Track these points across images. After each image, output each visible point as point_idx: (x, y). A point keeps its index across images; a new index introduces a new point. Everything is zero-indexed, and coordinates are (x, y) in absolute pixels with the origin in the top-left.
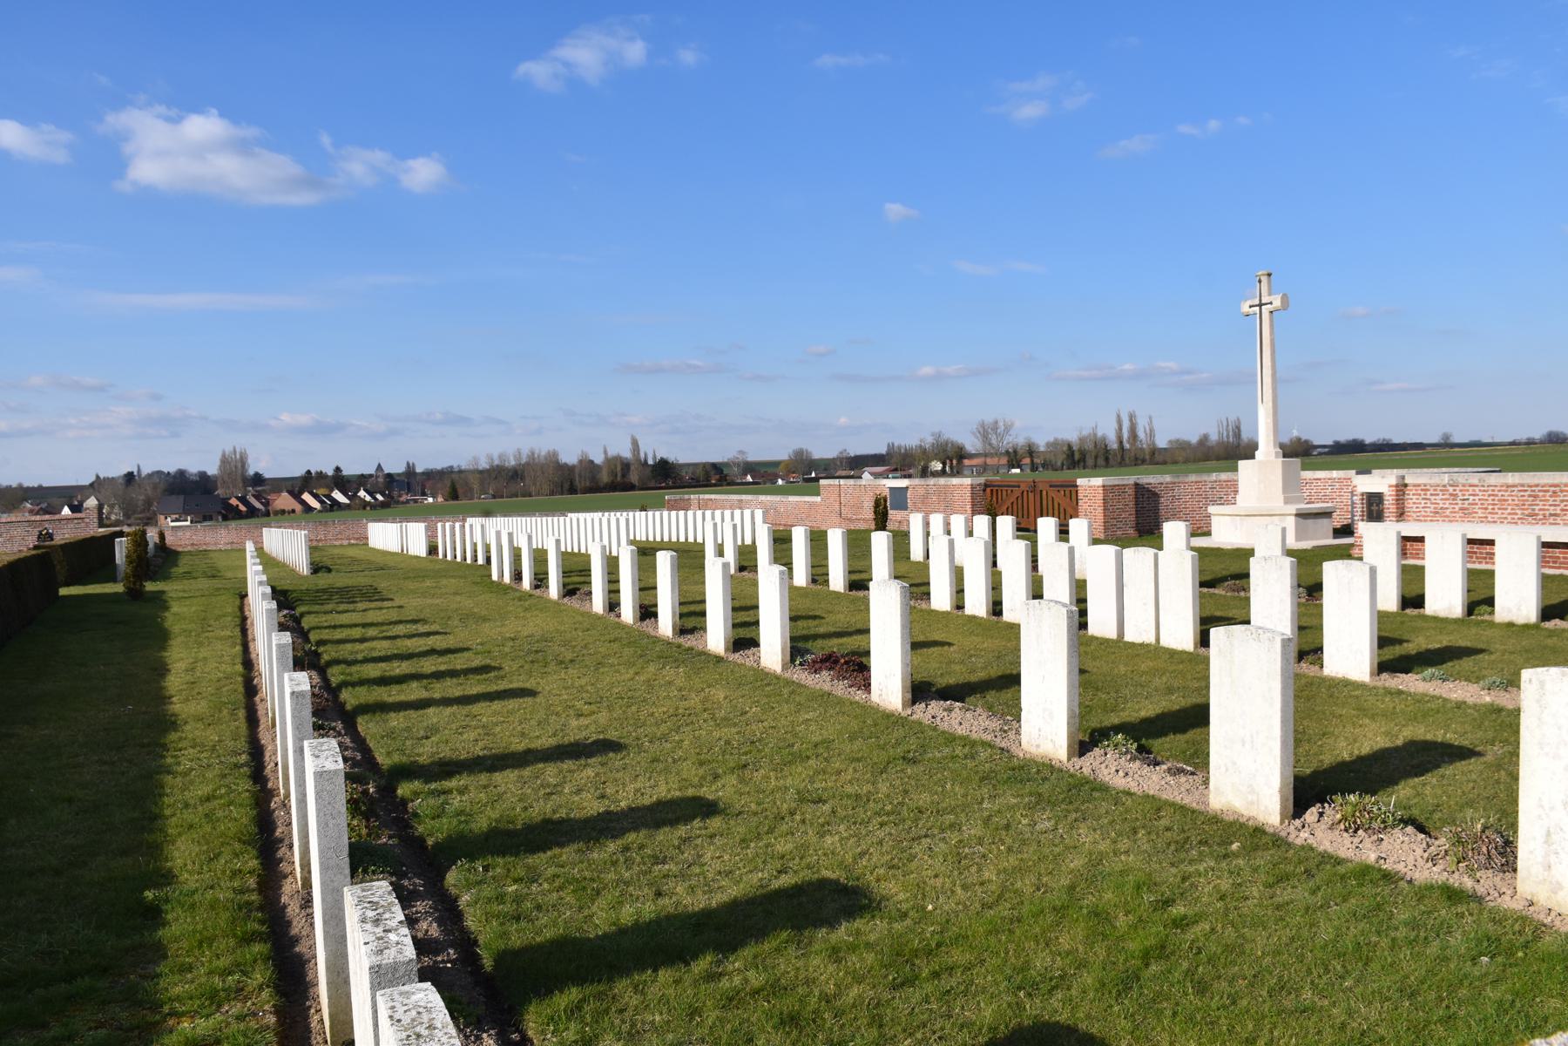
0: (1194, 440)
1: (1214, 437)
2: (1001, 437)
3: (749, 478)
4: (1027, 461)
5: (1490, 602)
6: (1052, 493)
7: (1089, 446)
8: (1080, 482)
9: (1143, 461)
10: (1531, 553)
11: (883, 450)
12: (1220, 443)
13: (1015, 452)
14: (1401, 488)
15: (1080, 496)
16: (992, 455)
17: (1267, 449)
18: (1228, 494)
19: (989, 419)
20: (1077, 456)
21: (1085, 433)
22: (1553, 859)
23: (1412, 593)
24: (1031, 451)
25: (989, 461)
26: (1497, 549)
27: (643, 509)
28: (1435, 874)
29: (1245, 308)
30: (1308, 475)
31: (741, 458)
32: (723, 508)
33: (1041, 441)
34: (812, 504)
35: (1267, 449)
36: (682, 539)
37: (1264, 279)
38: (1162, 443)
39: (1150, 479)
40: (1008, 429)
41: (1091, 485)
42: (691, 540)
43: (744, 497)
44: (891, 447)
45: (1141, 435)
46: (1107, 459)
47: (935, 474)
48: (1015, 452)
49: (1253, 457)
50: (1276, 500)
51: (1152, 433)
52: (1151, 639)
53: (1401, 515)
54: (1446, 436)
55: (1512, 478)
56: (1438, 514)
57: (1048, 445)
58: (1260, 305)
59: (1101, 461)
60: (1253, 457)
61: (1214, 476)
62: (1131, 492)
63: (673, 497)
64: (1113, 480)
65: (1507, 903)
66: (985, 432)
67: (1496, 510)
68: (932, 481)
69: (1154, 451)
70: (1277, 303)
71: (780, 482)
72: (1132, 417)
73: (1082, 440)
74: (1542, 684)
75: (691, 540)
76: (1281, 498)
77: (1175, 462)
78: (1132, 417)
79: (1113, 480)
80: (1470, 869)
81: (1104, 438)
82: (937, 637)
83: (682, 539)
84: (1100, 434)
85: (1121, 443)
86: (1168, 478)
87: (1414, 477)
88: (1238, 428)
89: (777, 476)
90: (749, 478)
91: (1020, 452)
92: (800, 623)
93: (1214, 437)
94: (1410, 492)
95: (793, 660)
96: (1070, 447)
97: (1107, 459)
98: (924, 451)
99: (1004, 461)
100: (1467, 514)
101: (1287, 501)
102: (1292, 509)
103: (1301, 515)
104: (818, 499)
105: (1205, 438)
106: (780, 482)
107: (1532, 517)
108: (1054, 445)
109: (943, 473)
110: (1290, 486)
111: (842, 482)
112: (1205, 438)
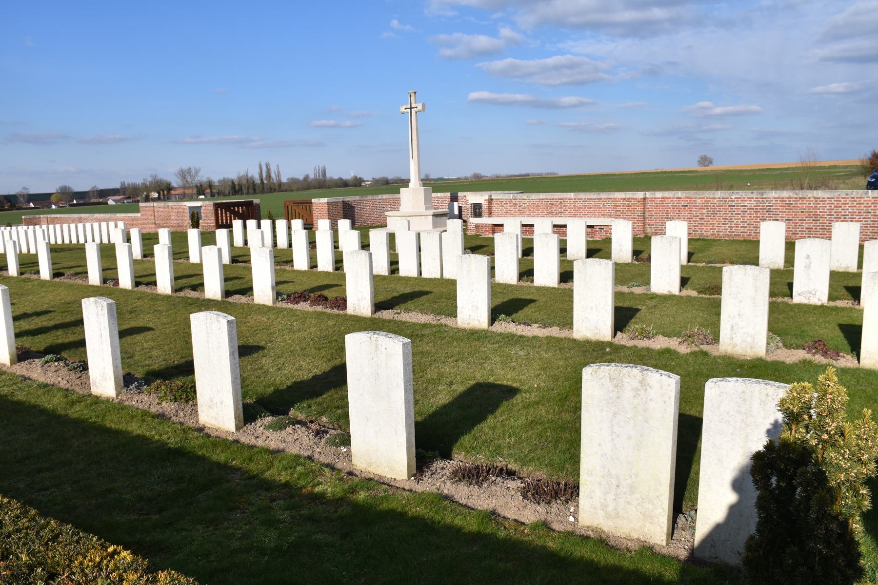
0: (301, 178)
1: (312, 176)
2: (193, 178)
3: (32, 205)
4: (208, 191)
5: (316, 266)
6: (294, 207)
7: (244, 182)
8: (313, 200)
9: (275, 190)
10: (583, 230)
11: (118, 186)
12: (315, 180)
13: (201, 186)
14: (490, 200)
15: (314, 208)
16: (188, 188)
17: (415, 182)
18: (395, 205)
19: (185, 167)
20: (237, 188)
21: (241, 175)
22: (734, 335)
23: (313, 264)
24: (210, 185)
25: (186, 191)
26: (535, 228)
27: (10, 225)
28: (689, 351)
29: (402, 109)
30: (434, 195)
31: (25, 192)
32: (61, 224)
33: (216, 179)
34: (133, 219)
35: (415, 182)
36: (59, 242)
37: (413, 95)
38: (284, 180)
39: (349, 199)
40: (197, 172)
41: (320, 203)
42: (74, 241)
43: (83, 215)
44: (123, 184)
45: (273, 175)
46: (254, 189)
47: (154, 200)
48: (201, 186)
49: (407, 186)
50: (422, 209)
51: (279, 175)
52: (439, 276)
53: (490, 214)
54: (705, 160)
55: (542, 196)
56: (508, 213)
57: (220, 181)
58: (411, 108)
59: (251, 191)
60: (407, 186)
61: (380, 197)
62: (341, 205)
63: (27, 217)
64: (332, 199)
65: (716, 354)
66: (183, 174)
67: (535, 210)
68: (151, 204)
69: (280, 184)
70: (420, 107)
71: (54, 207)
72: (267, 166)
73: (240, 178)
74: (731, 272)
75: (67, 241)
76: (424, 207)
77: (292, 191)
78: (267, 166)
79: (332, 199)
80: (696, 345)
81: (252, 178)
82: (335, 283)
83: (67, 241)
84: (250, 175)
85: (262, 180)
86: (358, 198)
87: (497, 195)
88: (325, 171)
89: (51, 204)
90: (32, 205)
91: (204, 186)
92: (230, 283)
93: (312, 176)
94: (494, 203)
95: (277, 299)
96: (233, 183)
97: (254, 189)
98: (146, 187)
99: (195, 191)
100: (521, 213)
101: (427, 209)
102: (431, 212)
103: (435, 216)
104: (139, 215)
105: (307, 177)
106: (54, 207)
107: (551, 214)
108: (224, 182)
109: (158, 199)
110: (427, 200)
111: (155, 204)
112: (307, 177)
